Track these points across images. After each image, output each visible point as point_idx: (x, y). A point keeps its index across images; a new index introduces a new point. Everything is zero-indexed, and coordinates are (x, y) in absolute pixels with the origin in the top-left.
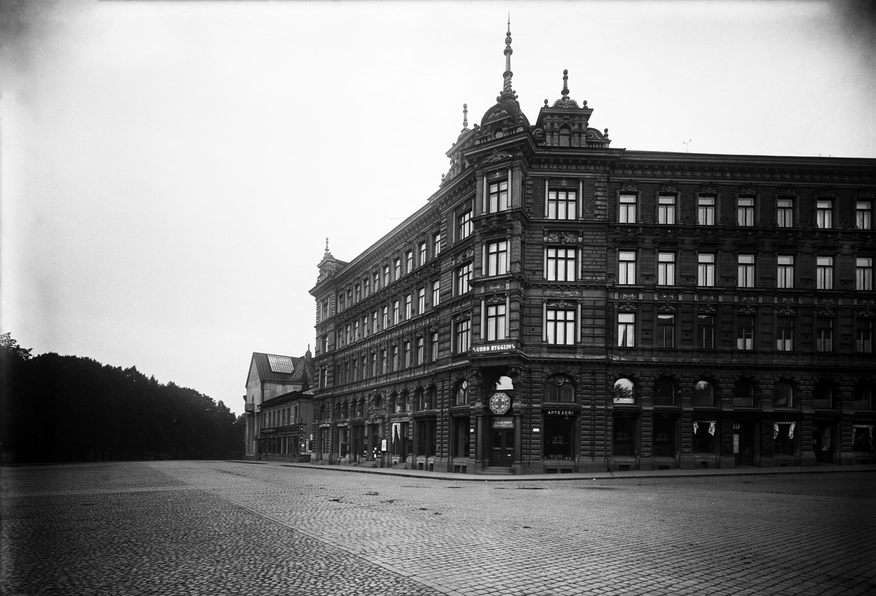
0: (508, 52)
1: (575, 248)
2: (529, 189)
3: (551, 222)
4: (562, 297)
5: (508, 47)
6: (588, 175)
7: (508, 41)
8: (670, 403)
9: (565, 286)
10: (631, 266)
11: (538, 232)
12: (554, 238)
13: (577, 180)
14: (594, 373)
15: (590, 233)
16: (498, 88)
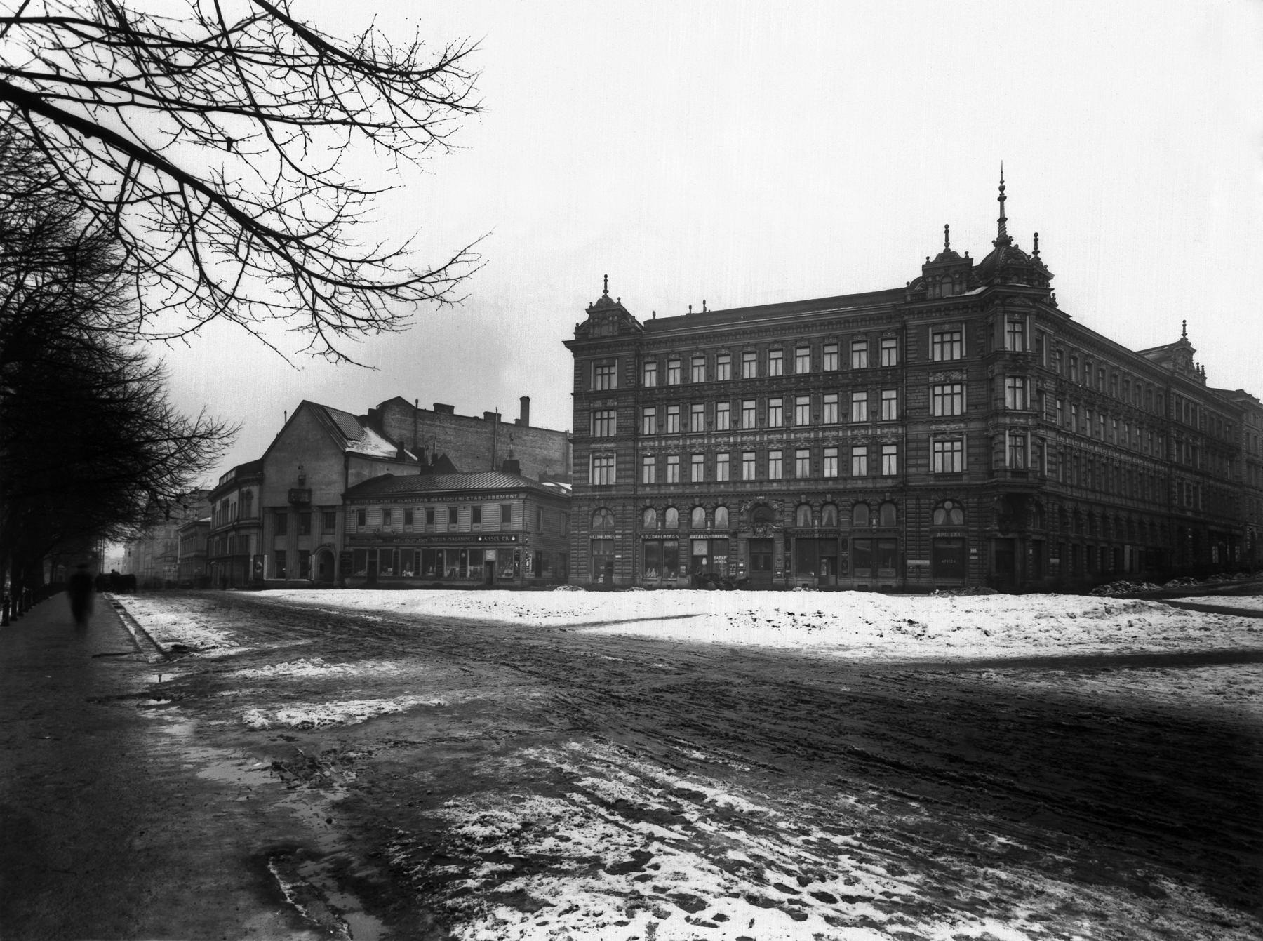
0: (1002, 199)
1: (960, 383)
4: (945, 428)
5: (1002, 194)
7: (1002, 189)
9: (953, 419)
10: (835, 407)
12: (940, 377)
13: (614, 358)
14: (624, 505)
16: (994, 235)
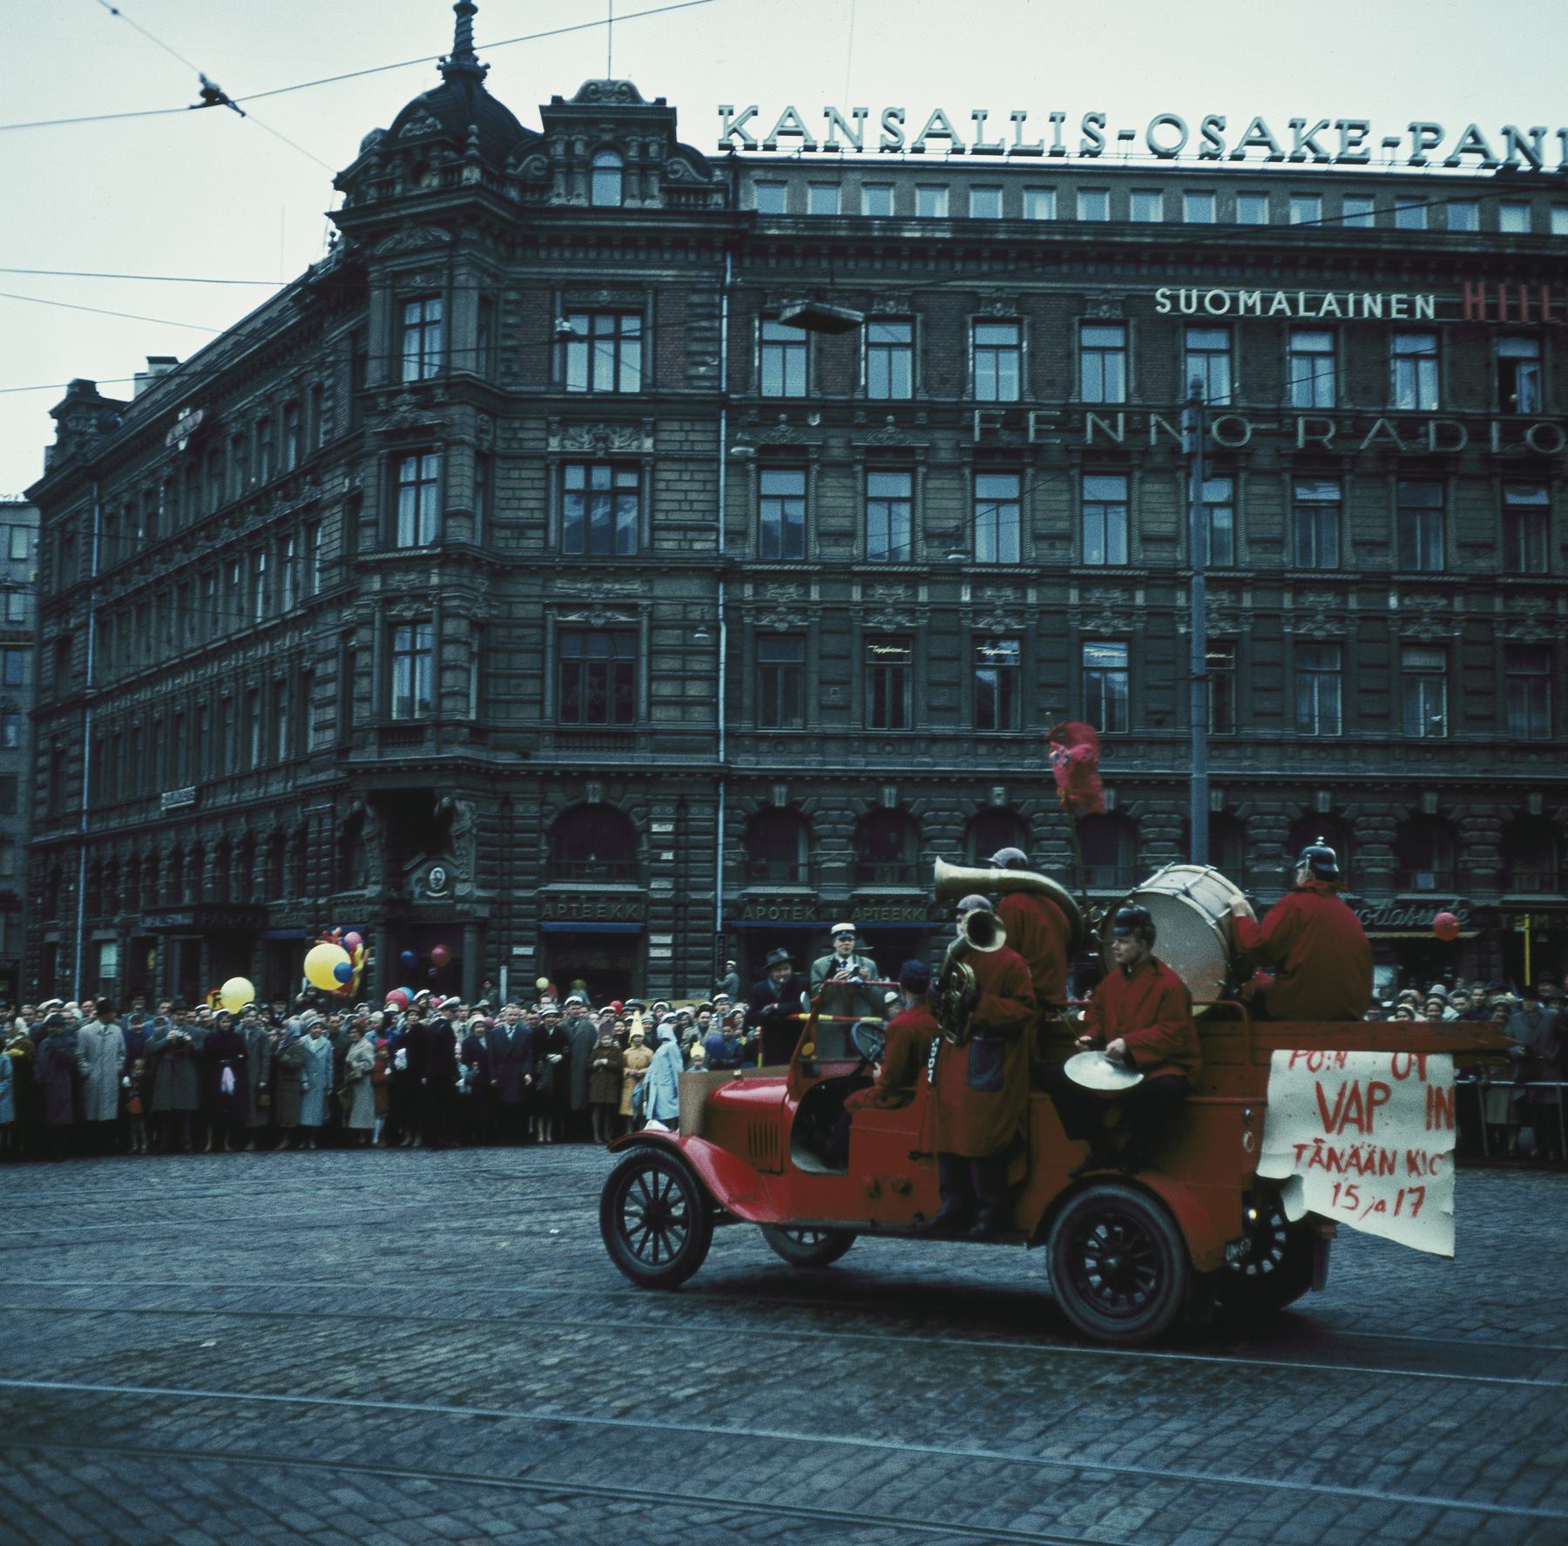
2: (509, 313)
3: (577, 398)
6: (668, 274)
8: (792, 879)
11: (531, 424)
15: (676, 426)
